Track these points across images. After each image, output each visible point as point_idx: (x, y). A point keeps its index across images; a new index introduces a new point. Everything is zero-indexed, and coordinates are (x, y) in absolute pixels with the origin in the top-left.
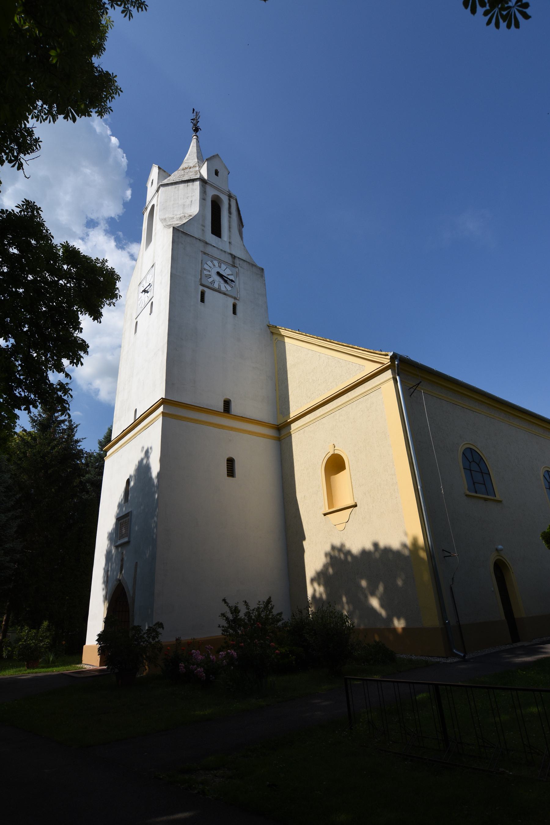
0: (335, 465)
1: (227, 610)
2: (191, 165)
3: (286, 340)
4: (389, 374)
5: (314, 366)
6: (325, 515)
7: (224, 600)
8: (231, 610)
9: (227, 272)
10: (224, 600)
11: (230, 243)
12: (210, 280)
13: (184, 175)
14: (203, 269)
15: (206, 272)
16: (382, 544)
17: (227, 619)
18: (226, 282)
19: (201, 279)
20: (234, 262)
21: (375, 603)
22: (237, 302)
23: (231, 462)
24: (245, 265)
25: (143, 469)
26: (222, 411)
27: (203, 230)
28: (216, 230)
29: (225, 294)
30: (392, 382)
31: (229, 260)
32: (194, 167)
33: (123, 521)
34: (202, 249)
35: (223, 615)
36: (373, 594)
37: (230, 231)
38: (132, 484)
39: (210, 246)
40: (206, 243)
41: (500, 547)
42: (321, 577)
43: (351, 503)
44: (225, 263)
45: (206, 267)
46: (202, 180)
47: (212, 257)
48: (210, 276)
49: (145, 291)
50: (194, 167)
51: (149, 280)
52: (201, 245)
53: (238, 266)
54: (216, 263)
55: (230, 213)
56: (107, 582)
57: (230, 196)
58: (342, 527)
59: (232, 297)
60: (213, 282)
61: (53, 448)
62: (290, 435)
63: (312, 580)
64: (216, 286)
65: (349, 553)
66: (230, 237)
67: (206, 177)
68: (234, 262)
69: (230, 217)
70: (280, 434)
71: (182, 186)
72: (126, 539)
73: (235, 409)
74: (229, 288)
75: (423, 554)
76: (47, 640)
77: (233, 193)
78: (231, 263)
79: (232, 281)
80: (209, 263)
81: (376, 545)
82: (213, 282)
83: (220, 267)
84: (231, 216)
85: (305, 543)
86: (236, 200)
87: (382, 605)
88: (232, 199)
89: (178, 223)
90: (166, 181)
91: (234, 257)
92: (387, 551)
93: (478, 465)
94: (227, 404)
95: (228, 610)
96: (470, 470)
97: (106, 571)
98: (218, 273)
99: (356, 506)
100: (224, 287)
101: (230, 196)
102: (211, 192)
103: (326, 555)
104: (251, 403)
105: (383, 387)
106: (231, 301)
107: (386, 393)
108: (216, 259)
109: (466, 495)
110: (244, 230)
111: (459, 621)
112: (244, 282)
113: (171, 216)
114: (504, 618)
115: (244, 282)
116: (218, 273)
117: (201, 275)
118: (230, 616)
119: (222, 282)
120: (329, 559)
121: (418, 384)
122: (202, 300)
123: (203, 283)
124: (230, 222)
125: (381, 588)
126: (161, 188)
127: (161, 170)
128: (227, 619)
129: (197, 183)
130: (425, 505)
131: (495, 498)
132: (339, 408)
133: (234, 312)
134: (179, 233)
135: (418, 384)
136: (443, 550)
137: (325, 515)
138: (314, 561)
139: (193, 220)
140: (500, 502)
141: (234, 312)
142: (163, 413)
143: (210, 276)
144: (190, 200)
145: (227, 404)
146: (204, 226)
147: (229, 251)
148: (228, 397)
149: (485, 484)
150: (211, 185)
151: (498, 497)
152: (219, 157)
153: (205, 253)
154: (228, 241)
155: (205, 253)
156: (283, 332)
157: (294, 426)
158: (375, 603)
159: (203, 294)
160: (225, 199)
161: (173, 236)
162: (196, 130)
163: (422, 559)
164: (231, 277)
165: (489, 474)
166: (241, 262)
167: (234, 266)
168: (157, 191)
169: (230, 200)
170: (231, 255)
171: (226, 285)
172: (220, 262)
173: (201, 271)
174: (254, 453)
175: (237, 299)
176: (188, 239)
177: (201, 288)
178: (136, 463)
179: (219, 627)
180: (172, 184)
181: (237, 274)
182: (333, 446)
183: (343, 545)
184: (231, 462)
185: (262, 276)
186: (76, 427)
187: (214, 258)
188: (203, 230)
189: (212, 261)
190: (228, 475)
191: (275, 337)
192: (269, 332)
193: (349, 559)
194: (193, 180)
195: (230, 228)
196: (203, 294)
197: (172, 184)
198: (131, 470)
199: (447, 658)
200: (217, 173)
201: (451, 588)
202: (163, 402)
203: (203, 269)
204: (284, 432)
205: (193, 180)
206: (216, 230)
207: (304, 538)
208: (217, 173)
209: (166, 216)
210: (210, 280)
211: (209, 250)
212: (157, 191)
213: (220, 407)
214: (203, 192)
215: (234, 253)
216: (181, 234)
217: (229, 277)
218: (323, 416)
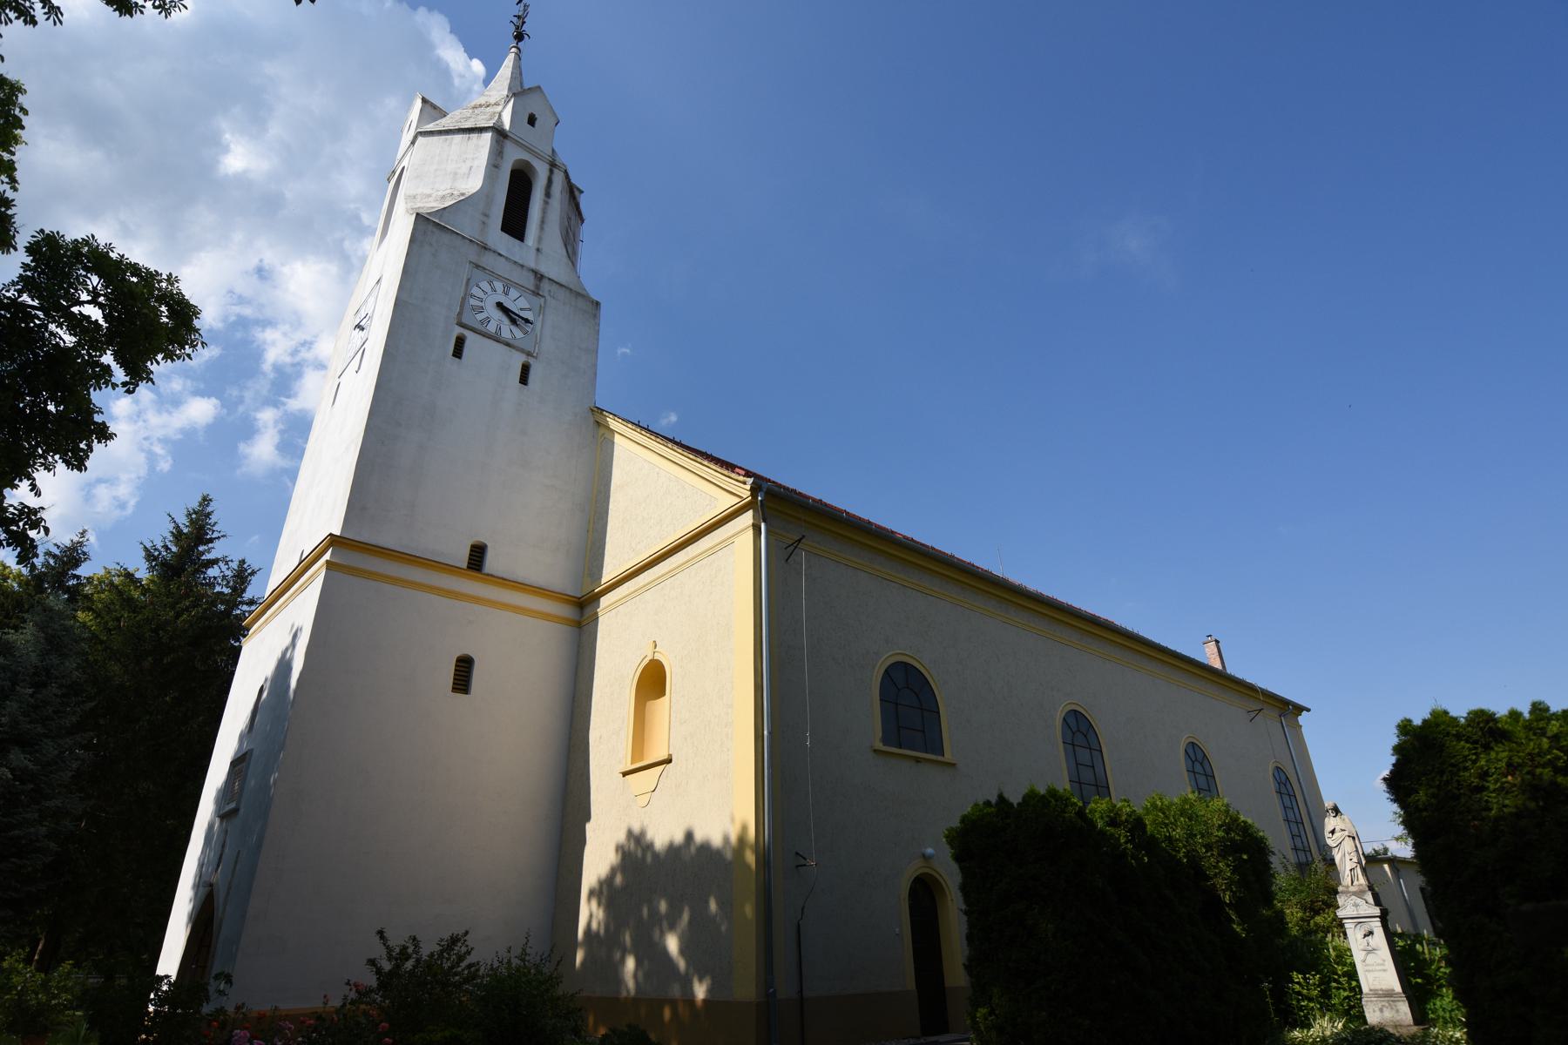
0: (653, 681)
1: (379, 951)
2: (492, 101)
3: (617, 438)
4: (748, 518)
5: (657, 492)
6: (625, 774)
7: (381, 933)
8: (389, 949)
9: (517, 303)
10: (381, 933)
12: (480, 317)
13: (467, 119)
14: (467, 295)
15: (473, 302)
16: (699, 837)
17: (379, 971)
18: (514, 322)
19: (460, 314)
20: (538, 287)
21: (672, 944)
22: (531, 360)
25: (284, 666)
26: (465, 565)
28: (515, 223)
29: (508, 344)
30: (750, 533)
31: (529, 282)
32: (497, 104)
33: (239, 764)
34: (473, 258)
35: (372, 962)
36: (672, 927)
38: (265, 695)
40: (485, 248)
41: (930, 851)
42: (607, 892)
43: (664, 756)
44: (518, 286)
45: (475, 291)
46: (499, 133)
48: (481, 310)
49: (359, 327)
50: (497, 104)
51: (368, 309)
52: (472, 253)
54: (499, 286)
55: (548, 194)
56: (197, 886)
57: (553, 165)
58: (644, 800)
59: (522, 351)
60: (488, 320)
61: (178, 616)
62: (595, 619)
63: (592, 893)
64: (492, 328)
65: (650, 846)
66: (540, 239)
67: (507, 126)
68: (538, 287)
69: (546, 203)
70: (582, 614)
71: (458, 138)
72: (233, 805)
73: (492, 563)
74: (518, 333)
75: (750, 858)
76: (64, 996)
77: (563, 158)
79: (527, 321)
80: (485, 285)
81: (689, 836)
82: (488, 320)
85: (588, 826)
87: (683, 951)
89: (431, 205)
90: (430, 127)
91: (539, 276)
92: (705, 848)
95: (384, 952)
97: (201, 865)
98: (500, 305)
99: (669, 761)
100: (507, 330)
101: (553, 165)
102: (513, 155)
103: (619, 848)
104: (529, 550)
105: (737, 540)
106: (518, 360)
107: (738, 554)
108: (499, 278)
110: (586, 231)
111: (801, 991)
112: (553, 326)
113: (428, 191)
114: (911, 984)
115: (553, 326)
116: (500, 305)
117: (462, 306)
118: (387, 966)
119: (506, 321)
120: (623, 859)
123: (465, 321)
124: (544, 211)
125: (686, 917)
126: (420, 139)
128: (379, 971)
129: (488, 136)
130: (771, 766)
131: (940, 758)
132: (672, 574)
133: (524, 380)
134: (426, 224)
137: (625, 774)
138: (598, 859)
140: (954, 765)
141: (524, 380)
142: (329, 565)
143: (481, 310)
144: (468, 164)
145: (478, 555)
146: (486, 215)
147: (532, 265)
148: (482, 539)
150: (517, 143)
151: (948, 756)
153: (477, 266)
155: (477, 266)
156: (614, 424)
157: (605, 601)
158: (672, 944)
159: (460, 344)
160: (541, 170)
161: (414, 229)
162: (519, 37)
163: (748, 867)
164: (525, 314)
166: (554, 288)
167: (536, 294)
168: (413, 143)
169: (551, 171)
170: (535, 272)
171: (514, 328)
172: (508, 285)
173: (464, 299)
174: (515, 648)
176: (446, 238)
177: (458, 330)
178: (278, 654)
179: (348, 983)
180: (440, 133)
181: (542, 310)
183: (643, 833)
185: (596, 316)
186: (253, 573)
187: (493, 276)
189: (490, 283)
190: (455, 689)
191: (602, 431)
193: (649, 859)
194: (481, 130)
196: (460, 344)
197: (440, 133)
198: (268, 669)
200: (532, 120)
202: (333, 541)
204: (588, 611)
205: (481, 130)
206: (515, 223)
207: (588, 818)
208: (532, 120)
209: (420, 191)
210: (480, 317)
211: (488, 260)
212: (413, 143)
213: (462, 557)
214: (497, 154)
215: (543, 269)
216: (430, 227)
217: (522, 314)
218: (647, 588)
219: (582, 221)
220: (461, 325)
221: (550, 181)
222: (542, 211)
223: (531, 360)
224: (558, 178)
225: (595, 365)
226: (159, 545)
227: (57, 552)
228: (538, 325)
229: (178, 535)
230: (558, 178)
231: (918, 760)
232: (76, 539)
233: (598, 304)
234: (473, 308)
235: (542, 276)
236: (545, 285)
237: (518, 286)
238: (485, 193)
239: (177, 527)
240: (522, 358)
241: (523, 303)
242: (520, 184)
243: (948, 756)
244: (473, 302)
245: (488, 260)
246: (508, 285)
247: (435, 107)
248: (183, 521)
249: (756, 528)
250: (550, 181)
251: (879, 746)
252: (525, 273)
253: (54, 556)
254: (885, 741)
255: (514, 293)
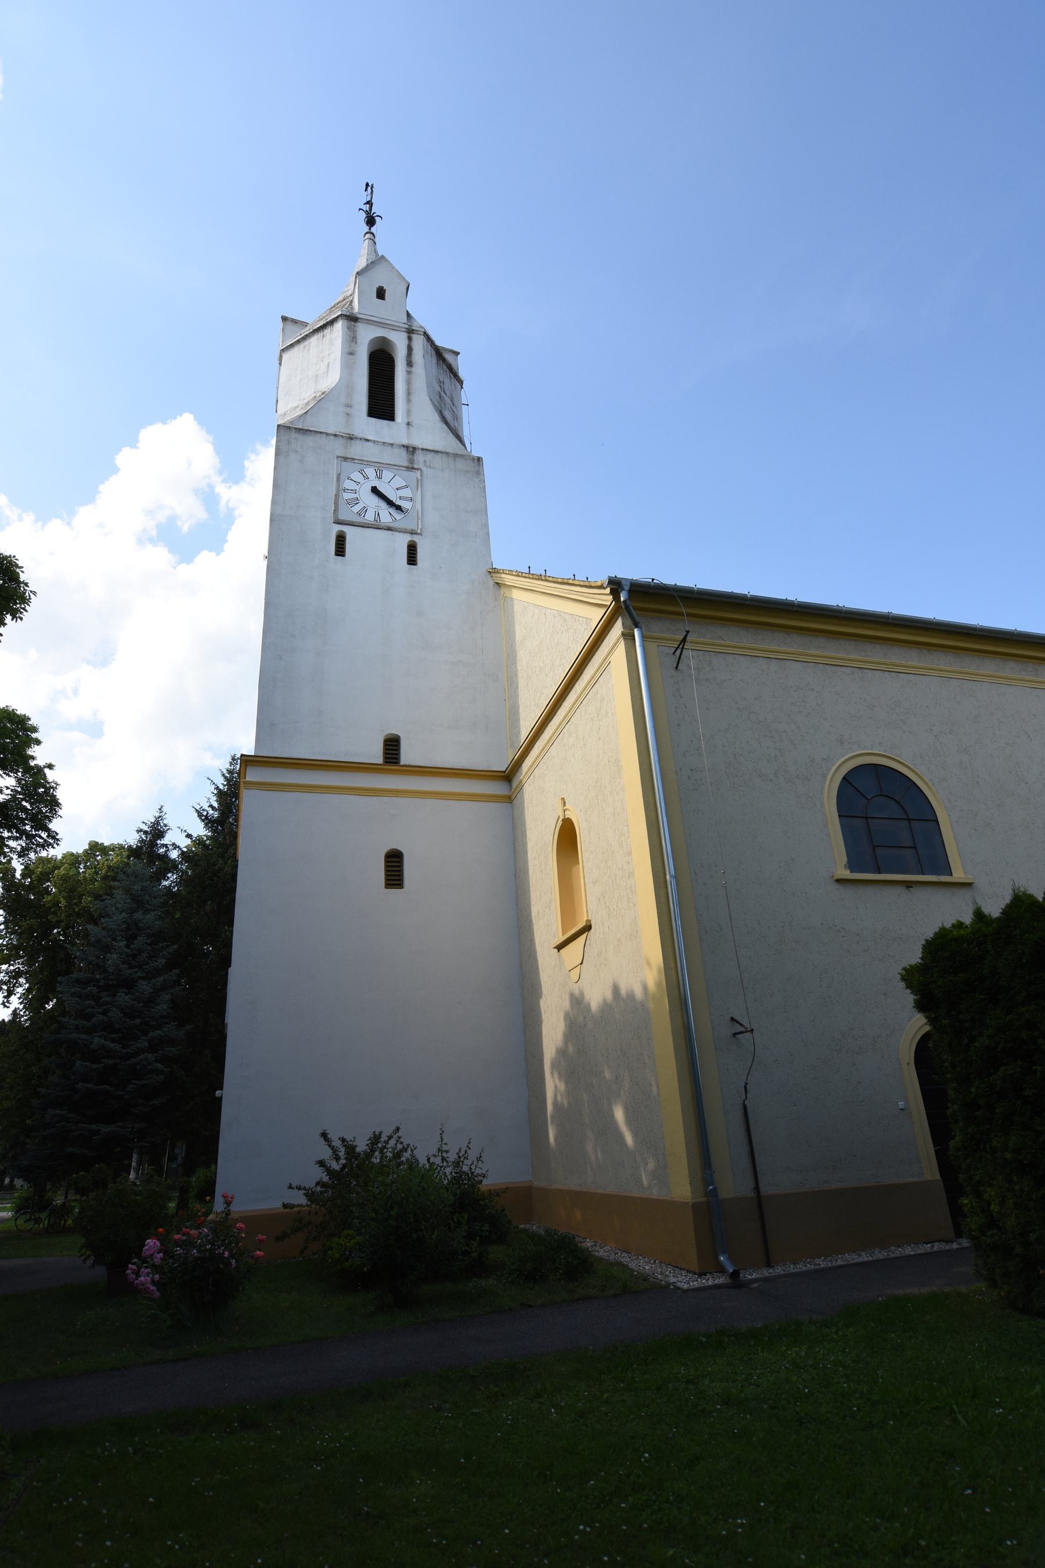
1: (326, 1153)
3: (516, 594)
6: (560, 947)
10: (324, 1135)
11: (408, 424)
14: (339, 491)
15: (347, 496)
19: (336, 511)
20: (411, 461)
22: (416, 538)
23: (394, 861)
24: (438, 461)
26: (380, 761)
27: (348, 414)
28: (381, 404)
29: (389, 529)
30: (622, 647)
31: (402, 458)
35: (321, 1163)
37: (409, 400)
39: (358, 441)
40: (351, 438)
44: (390, 466)
45: (348, 484)
47: (361, 461)
52: (338, 447)
53: (421, 466)
54: (370, 472)
55: (410, 363)
57: (410, 332)
59: (405, 531)
64: (370, 517)
66: (409, 412)
68: (411, 461)
69: (409, 373)
71: (314, 340)
73: (407, 756)
77: (421, 320)
78: (406, 464)
80: (357, 476)
82: (365, 510)
83: (380, 478)
84: (413, 369)
86: (425, 334)
88: (414, 336)
93: (898, 803)
94: (392, 746)
96: (908, 820)
98: (375, 490)
100: (387, 516)
102: (367, 335)
106: (402, 542)
108: (369, 463)
109: (838, 881)
115: (431, 500)
116: (375, 490)
117: (336, 504)
121: (684, 640)
122: (340, 549)
123: (342, 517)
124: (409, 382)
126: (286, 356)
127: (288, 323)
129: (339, 326)
132: (567, 720)
135: (684, 640)
136: (732, 1019)
137: (560, 947)
139: (322, 400)
140: (968, 885)
141: (412, 558)
144: (326, 361)
145: (392, 746)
146: (349, 406)
147: (405, 442)
149: (915, 848)
151: (958, 874)
152: (386, 260)
153: (345, 459)
154: (406, 421)
155: (345, 459)
162: (371, 221)
165: (937, 821)
166: (430, 456)
167: (411, 468)
169: (410, 339)
170: (406, 447)
172: (380, 468)
173: (337, 496)
175: (416, 534)
176: (310, 440)
182: (560, 803)
184: (394, 861)
188: (348, 414)
189: (361, 472)
191: (503, 590)
192: (491, 583)
195: (409, 394)
199: (701, 1274)
200: (381, 294)
201: (745, 1107)
203: (339, 491)
204: (515, 784)
205: (332, 323)
206: (381, 404)
208: (381, 294)
211: (356, 450)
213: (376, 754)
214: (352, 338)
216: (294, 435)
219: (461, 382)
220: (338, 522)
221: (410, 349)
222: (411, 386)
223: (416, 538)
224: (418, 342)
225: (486, 525)
226: (206, 807)
227: (146, 828)
228: (418, 499)
229: (220, 794)
230: (418, 342)
231: (909, 885)
232: (157, 815)
233: (479, 459)
234: (348, 502)
235: (414, 448)
236: (420, 457)
237: (390, 466)
238: (346, 385)
239: (217, 788)
240: (406, 538)
241: (399, 482)
242: (381, 365)
243: (958, 874)
244: (347, 496)
245: (356, 450)
246: (380, 468)
247: (295, 322)
248: (221, 782)
249: (628, 637)
250: (410, 349)
251: (847, 874)
252: (396, 450)
253: (146, 832)
254: (853, 864)
255: (387, 475)
